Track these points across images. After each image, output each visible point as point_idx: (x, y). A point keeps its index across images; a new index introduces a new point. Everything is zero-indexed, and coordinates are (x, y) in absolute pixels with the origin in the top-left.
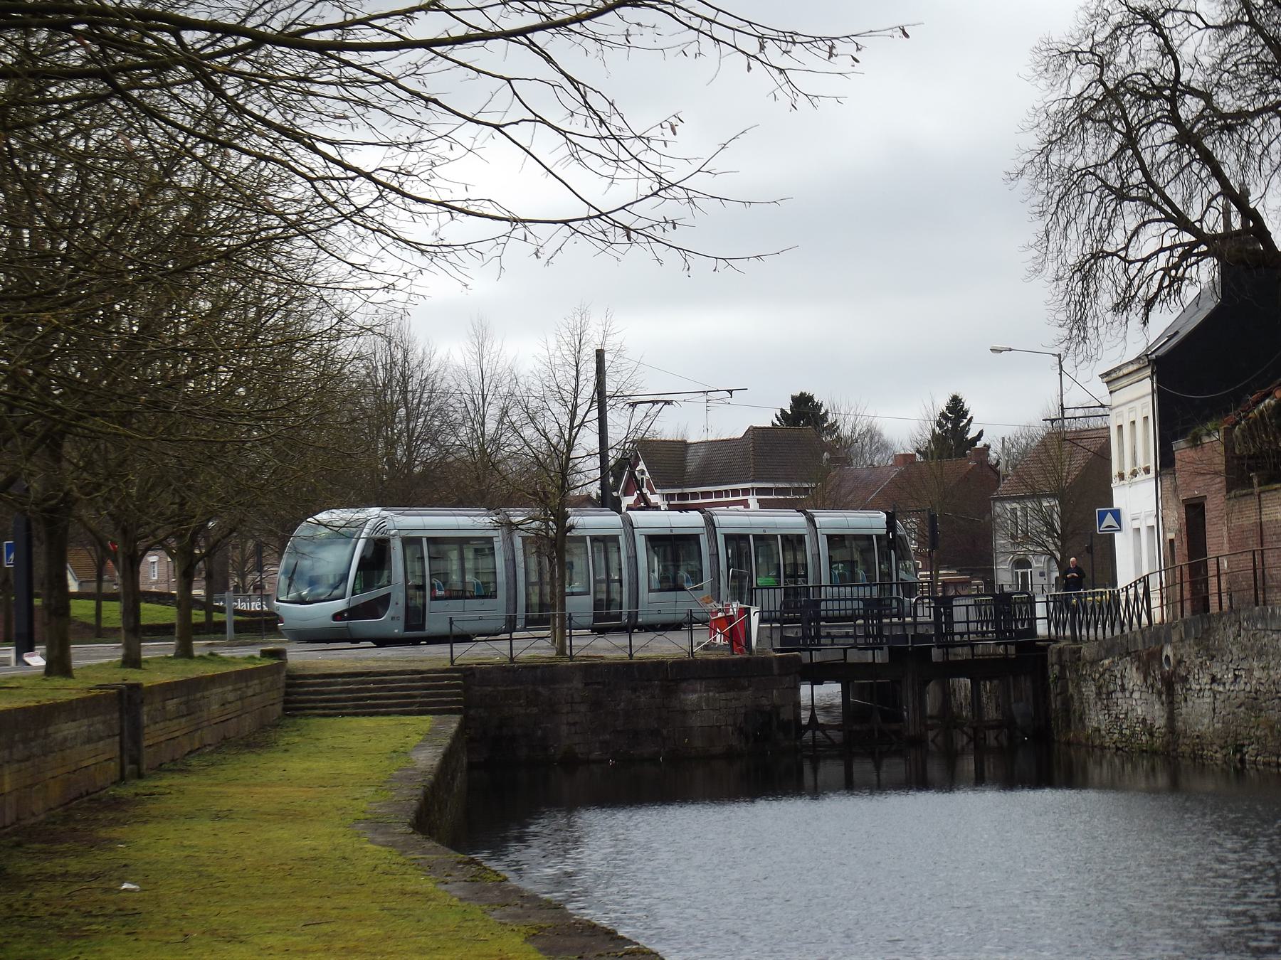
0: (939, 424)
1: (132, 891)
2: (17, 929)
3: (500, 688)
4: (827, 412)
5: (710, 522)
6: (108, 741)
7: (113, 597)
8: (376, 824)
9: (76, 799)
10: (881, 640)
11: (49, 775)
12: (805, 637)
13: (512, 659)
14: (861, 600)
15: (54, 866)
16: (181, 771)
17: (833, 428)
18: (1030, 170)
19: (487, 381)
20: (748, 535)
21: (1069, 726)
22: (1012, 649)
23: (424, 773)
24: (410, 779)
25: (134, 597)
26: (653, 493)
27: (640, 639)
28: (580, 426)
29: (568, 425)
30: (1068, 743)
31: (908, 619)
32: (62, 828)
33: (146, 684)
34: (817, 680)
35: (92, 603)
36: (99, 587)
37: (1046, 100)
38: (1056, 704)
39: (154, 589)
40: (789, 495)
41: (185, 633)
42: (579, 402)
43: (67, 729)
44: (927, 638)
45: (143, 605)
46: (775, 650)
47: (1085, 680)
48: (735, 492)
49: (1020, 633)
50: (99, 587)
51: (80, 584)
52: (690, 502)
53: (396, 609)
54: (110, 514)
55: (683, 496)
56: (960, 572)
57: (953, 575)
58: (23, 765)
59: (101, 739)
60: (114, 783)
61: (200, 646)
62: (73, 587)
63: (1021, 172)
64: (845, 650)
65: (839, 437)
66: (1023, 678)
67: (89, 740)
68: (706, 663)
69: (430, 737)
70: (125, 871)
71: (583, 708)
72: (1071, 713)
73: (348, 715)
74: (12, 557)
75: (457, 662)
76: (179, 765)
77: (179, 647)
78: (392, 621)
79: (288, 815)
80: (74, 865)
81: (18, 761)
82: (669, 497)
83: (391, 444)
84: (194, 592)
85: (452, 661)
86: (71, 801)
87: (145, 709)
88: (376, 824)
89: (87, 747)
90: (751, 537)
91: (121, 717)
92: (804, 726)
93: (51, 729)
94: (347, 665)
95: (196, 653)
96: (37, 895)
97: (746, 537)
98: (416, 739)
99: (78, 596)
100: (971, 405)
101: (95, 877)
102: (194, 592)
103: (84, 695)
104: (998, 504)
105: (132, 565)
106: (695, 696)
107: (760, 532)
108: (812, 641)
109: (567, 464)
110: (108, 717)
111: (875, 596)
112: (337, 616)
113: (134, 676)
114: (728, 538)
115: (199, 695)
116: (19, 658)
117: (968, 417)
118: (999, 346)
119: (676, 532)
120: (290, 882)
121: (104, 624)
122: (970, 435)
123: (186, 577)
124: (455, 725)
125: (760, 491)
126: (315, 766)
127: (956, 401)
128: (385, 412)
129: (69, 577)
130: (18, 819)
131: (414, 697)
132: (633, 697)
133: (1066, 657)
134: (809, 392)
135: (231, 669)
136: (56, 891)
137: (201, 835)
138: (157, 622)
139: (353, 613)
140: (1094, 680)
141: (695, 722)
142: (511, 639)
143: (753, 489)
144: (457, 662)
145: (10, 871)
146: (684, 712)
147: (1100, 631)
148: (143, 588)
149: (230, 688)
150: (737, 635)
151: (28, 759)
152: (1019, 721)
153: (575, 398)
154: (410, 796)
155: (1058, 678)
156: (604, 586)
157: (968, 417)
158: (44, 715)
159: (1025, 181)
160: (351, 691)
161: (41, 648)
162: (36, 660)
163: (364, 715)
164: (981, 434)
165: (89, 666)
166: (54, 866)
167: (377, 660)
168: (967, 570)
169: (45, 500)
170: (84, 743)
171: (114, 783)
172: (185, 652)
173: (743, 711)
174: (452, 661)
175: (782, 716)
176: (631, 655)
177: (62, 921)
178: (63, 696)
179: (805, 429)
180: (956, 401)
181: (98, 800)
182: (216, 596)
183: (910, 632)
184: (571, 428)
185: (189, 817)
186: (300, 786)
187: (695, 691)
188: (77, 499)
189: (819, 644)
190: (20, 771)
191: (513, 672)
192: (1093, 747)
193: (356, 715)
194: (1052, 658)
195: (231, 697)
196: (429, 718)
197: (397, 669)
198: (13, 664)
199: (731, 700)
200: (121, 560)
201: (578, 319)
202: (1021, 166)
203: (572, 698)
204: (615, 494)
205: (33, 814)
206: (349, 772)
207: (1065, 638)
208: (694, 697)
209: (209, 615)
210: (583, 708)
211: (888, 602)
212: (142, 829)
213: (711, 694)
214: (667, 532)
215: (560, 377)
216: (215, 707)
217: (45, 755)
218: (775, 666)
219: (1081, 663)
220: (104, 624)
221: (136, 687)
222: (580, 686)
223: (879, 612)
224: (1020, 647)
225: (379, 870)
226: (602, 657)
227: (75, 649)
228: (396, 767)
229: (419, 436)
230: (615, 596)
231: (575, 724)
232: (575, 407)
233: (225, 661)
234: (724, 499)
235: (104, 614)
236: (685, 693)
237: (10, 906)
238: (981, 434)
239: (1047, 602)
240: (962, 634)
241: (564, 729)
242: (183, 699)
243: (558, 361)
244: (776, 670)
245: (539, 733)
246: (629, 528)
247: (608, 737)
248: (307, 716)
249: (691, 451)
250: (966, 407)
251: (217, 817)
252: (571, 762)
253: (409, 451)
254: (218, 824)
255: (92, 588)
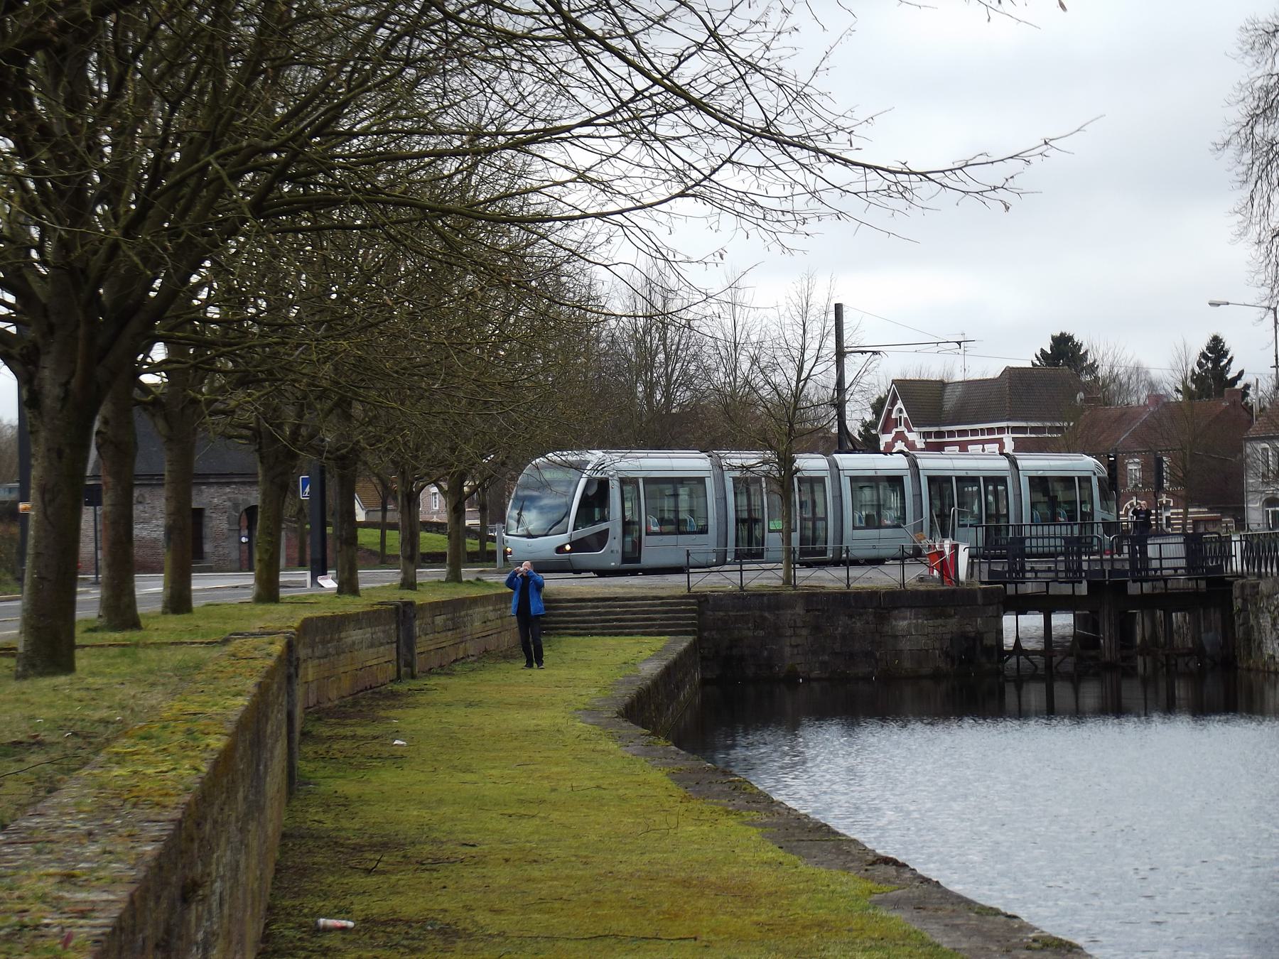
0: (1200, 364)
1: (402, 745)
2: (322, 764)
3: (731, 613)
4: (1086, 353)
5: (914, 465)
6: (387, 646)
7: (394, 527)
8: (591, 712)
9: (362, 691)
10: (1081, 575)
11: (342, 670)
12: (1010, 571)
13: (742, 587)
14: (1064, 538)
15: (348, 731)
16: (447, 674)
17: (1093, 368)
18: (1235, 141)
19: (739, 328)
20: (978, 477)
21: (1250, 654)
22: (1203, 584)
23: (644, 679)
24: (631, 683)
25: (412, 527)
26: (910, 431)
27: (855, 572)
28: (806, 379)
29: (795, 378)
30: (1249, 670)
31: (1106, 557)
32: (352, 710)
33: (418, 602)
34: (1021, 611)
35: (378, 532)
36: (384, 517)
37: (1251, 76)
38: (1240, 632)
39: (435, 519)
40: (1026, 433)
41: (455, 560)
42: (806, 357)
43: (354, 635)
44: (1124, 573)
45: (423, 534)
46: (982, 583)
47: (1263, 612)
48: (991, 431)
49: (1210, 570)
50: (384, 517)
51: (367, 513)
52: (947, 439)
53: (615, 544)
54: (393, 461)
55: (940, 434)
56: (1211, 511)
57: (1204, 513)
58: (322, 661)
59: (382, 644)
60: (391, 681)
61: (468, 573)
62: (361, 516)
63: (1227, 143)
64: (1047, 583)
65: (1097, 378)
66: (1212, 610)
67: (372, 645)
68: (915, 594)
69: (658, 654)
70: (397, 734)
71: (804, 632)
72: (1252, 642)
73: (596, 634)
74: (307, 490)
75: (693, 590)
76: (445, 669)
77: (450, 573)
78: (611, 553)
79: (522, 705)
80: (360, 731)
81: (319, 658)
82: (926, 435)
83: (651, 387)
84: (468, 523)
85: (689, 589)
86: (358, 692)
87: (417, 622)
88: (591, 712)
89: (371, 650)
90: (954, 479)
91: (398, 628)
92: (1008, 652)
93: (343, 635)
94: (597, 591)
95: (464, 579)
96: (335, 747)
97: (949, 479)
98: (648, 653)
99: (365, 525)
100: (1229, 343)
101: (375, 738)
102: (468, 523)
103: (369, 609)
104: (1248, 445)
105: (411, 501)
106: (905, 623)
107: (963, 474)
108: (1018, 575)
109: (794, 413)
110: (387, 627)
111: (1076, 532)
112: (560, 549)
113: (409, 596)
114: (931, 480)
115: (463, 613)
116: (314, 578)
117: (1229, 357)
118: (1217, 299)
119: (880, 473)
120: (516, 743)
121: (388, 552)
122: (1229, 376)
123: (457, 511)
124: (685, 644)
125: (1015, 430)
126: (556, 672)
127: (1216, 340)
128: (646, 356)
129: (357, 506)
130: (318, 702)
131: (655, 620)
132: (849, 622)
133: (1248, 591)
134: (1069, 332)
135: (493, 592)
136: (348, 745)
137: (457, 717)
138: (436, 550)
139: (578, 545)
140: (1269, 612)
141: (905, 645)
142: (741, 571)
143: (1008, 427)
144: (693, 590)
145: (314, 733)
146: (896, 637)
147: (1269, 570)
148: (422, 517)
149: (491, 608)
150: (947, 567)
151: (326, 657)
152: (1208, 648)
153: (803, 354)
154: (626, 693)
155: (1240, 611)
156: (810, 524)
157: (1229, 357)
158: (337, 623)
159: (1231, 152)
160: (600, 614)
161: (332, 572)
162: (329, 583)
163: (610, 635)
164: (1241, 374)
165: (373, 588)
166: (348, 731)
167: (622, 587)
168: (1217, 508)
169: (338, 450)
170: (369, 647)
171: (391, 681)
172: (455, 577)
173: (949, 636)
174: (689, 589)
175: (985, 642)
176: (848, 586)
177: (352, 761)
178: (352, 609)
179: (1063, 369)
180: (1216, 340)
181: (380, 693)
182: (490, 526)
183: (1107, 567)
184: (798, 381)
185: (448, 705)
186: (539, 686)
187: (904, 619)
188: (364, 449)
189: (1024, 577)
190: (320, 665)
191: (743, 600)
192: (1269, 672)
193: (603, 635)
194: (1236, 592)
195: (491, 616)
196: (667, 638)
197: (640, 595)
198: (309, 586)
199: (938, 627)
200: (400, 498)
201: (805, 283)
202: (1227, 138)
203: (795, 622)
204: (873, 432)
205: (329, 699)
206: (583, 677)
207: (1254, 573)
208: (904, 623)
209: (483, 544)
210: (804, 632)
211: (1089, 540)
212: (411, 712)
213: (920, 621)
214: (872, 473)
215: (789, 335)
216: (477, 624)
217: (338, 654)
218: (979, 595)
219: (1258, 597)
220: (388, 552)
221: (410, 604)
222: (802, 612)
223: (1079, 549)
224: (1210, 582)
225: (582, 737)
226: (823, 587)
227: (362, 573)
228: (623, 674)
229: (677, 379)
230: (821, 533)
231: (797, 646)
232: (802, 362)
233: (489, 585)
234: (980, 437)
235: (388, 542)
236: (896, 620)
237: (316, 752)
238: (1241, 374)
239: (1241, 541)
240: (1156, 570)
241: (787, 651)
242: (449, 616)
243: (787, 321)
244: (980, 601)
245: (766, 653)
246: (835, 470)
247: (826, 658)
248: (559, 635)
249: (948, 390)
250: (1226, 347)
251: (470, 705)
252: (791, 679)
253: (668, 395)
254: (469, 710)
255: (377, 517)
